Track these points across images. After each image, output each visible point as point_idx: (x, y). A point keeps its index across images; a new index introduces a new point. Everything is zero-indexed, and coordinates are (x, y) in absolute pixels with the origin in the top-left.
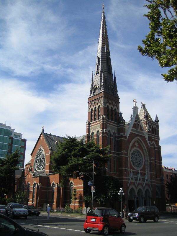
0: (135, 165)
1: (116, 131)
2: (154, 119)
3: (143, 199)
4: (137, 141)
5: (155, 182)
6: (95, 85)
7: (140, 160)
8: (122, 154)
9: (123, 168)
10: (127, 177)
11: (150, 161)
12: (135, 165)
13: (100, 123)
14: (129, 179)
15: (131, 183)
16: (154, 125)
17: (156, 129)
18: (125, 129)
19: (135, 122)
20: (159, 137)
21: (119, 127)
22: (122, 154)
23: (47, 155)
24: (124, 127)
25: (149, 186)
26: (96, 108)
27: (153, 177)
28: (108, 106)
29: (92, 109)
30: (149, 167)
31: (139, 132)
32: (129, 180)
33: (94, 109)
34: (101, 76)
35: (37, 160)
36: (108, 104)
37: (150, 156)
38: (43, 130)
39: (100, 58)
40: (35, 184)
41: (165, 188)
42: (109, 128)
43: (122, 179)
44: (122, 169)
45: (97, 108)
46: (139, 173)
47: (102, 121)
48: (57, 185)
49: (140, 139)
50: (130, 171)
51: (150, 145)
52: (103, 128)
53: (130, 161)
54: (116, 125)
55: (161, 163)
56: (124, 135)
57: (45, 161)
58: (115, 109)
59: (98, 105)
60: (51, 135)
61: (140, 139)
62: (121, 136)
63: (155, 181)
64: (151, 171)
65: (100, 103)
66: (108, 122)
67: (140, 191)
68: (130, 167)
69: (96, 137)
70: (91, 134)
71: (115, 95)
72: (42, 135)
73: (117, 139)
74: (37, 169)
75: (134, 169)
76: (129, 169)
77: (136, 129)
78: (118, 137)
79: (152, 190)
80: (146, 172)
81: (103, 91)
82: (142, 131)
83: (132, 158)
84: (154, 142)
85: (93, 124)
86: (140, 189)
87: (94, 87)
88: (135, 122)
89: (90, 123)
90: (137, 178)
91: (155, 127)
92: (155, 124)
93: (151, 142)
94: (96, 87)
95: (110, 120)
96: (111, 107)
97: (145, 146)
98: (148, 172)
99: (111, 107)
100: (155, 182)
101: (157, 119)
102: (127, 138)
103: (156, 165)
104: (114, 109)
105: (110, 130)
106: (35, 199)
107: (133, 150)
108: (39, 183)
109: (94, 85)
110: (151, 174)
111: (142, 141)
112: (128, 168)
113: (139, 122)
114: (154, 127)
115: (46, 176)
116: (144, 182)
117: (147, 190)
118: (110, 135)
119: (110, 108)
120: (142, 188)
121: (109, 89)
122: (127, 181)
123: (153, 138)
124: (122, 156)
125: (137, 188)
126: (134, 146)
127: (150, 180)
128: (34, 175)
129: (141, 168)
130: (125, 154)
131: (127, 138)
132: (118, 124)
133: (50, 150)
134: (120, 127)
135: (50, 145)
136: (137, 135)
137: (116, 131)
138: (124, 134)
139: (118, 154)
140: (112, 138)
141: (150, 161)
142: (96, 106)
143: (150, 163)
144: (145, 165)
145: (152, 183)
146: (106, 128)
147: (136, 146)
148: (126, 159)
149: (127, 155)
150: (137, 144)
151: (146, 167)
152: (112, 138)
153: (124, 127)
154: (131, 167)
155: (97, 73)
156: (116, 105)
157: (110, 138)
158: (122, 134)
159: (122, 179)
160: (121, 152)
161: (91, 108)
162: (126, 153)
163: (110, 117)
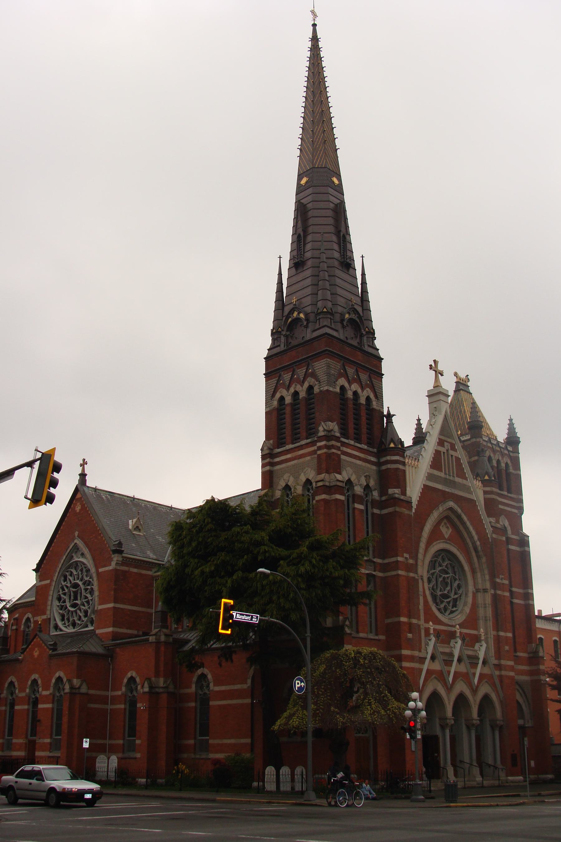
0: (442, 606)
1: (372, 483)
2: (501, 435)
3: (448, 732)
4: (447, 518)
5: (512, 669)
7: (459, 587)
8: (396, 566)
9: (403, 619)
10: (416, 653)
11: (492, 591)
12: (442, 606)
13: (315, 452)
14: (422, 660)
16: (503, 455)
17: (511, 470)
18: (404, 471)
19: (440, 449)
20: (521, 501)
21: (384, 467)
22: (396, 566)
23: (101, 570)
24: (401, 467)
25: (493, 685)
26: (296, 394)
27: (507, 648)
28: (342, 388)
29: (282, 399)
30: (490, 612)
31: (452, 484)
32: (423, 663)
33: (288, 400)
37: (493, 576)
38: (83, 476)
41: (548, 690)
43: (399, 658)
44: (399, 622)
48: (146, 685)
50: (427, 630)
51: (494, 532)
53: (424, 592)
54: (373, 459)
55: (529, 596)
56: (402, 497)
57: (96, 593)
58: (368, 399)
61: (459, 511)
62: (394, 501)
63: (511, 663)
64: (497, 627)
65: (314, 375)
66: (345, 449)
67: (461, 700)
71: (366, 348)
73: (376, 511)
74: (60, 624)
75: (437, 621)
76: (422, 622)
77: (442, 474)
78: (381, 505)
79: (501, 695)
80: (482, 630)
82: (464, 482)
83: (429, 581)
85: (289, 456)
87: (288, 317)
88: (440, 449)
90: (451, 655)
91: (507, 464)
92: (506, 452)
93: (497, 522)
94: (295, 314)
95: (352, 442)
96: (355, 393)
97: (474, 533)
98: (486, 634)
99: (355, 393)
100: (512, 669)
102: (414, 505)
103: (511, 603)
104: (363, 401)
105: (353, 478)
109: (287, 309)
110: (498, 639)
112: (419, 619)
114: (503, 465)
116: (451, 666)
117: (486, 698)
118: (354, 496)
120: (468, 693)
121: (345, 323)
122: (416, 665)
123: (501, 507)
124: (398, 575)
125: (449, 689)
126: (435, 535)
127: (496, 662)
129: (460, 618)
131: (414, 505)
132: (378, 455)
134: (389, 466)
136: (446, 496)
137: (372, 483)
138: (404, 493)
139: (384, 568)
140: (362, 507)
141: (492, 591)
142: (299, 388)
143: (495, 598)
145: (504, 673)
147: (444, 538)
148: (413, 583)
149: (413, 568)
150: (446, 531)
152: (362, 507)
153: (401, 467)
154: (430, 617)
156: (371, 382)
158: (394, 491)
159: (399, 658)
160: (393, 559)
161: (278, 395)
162: (411, 561)
163: (351, 431)
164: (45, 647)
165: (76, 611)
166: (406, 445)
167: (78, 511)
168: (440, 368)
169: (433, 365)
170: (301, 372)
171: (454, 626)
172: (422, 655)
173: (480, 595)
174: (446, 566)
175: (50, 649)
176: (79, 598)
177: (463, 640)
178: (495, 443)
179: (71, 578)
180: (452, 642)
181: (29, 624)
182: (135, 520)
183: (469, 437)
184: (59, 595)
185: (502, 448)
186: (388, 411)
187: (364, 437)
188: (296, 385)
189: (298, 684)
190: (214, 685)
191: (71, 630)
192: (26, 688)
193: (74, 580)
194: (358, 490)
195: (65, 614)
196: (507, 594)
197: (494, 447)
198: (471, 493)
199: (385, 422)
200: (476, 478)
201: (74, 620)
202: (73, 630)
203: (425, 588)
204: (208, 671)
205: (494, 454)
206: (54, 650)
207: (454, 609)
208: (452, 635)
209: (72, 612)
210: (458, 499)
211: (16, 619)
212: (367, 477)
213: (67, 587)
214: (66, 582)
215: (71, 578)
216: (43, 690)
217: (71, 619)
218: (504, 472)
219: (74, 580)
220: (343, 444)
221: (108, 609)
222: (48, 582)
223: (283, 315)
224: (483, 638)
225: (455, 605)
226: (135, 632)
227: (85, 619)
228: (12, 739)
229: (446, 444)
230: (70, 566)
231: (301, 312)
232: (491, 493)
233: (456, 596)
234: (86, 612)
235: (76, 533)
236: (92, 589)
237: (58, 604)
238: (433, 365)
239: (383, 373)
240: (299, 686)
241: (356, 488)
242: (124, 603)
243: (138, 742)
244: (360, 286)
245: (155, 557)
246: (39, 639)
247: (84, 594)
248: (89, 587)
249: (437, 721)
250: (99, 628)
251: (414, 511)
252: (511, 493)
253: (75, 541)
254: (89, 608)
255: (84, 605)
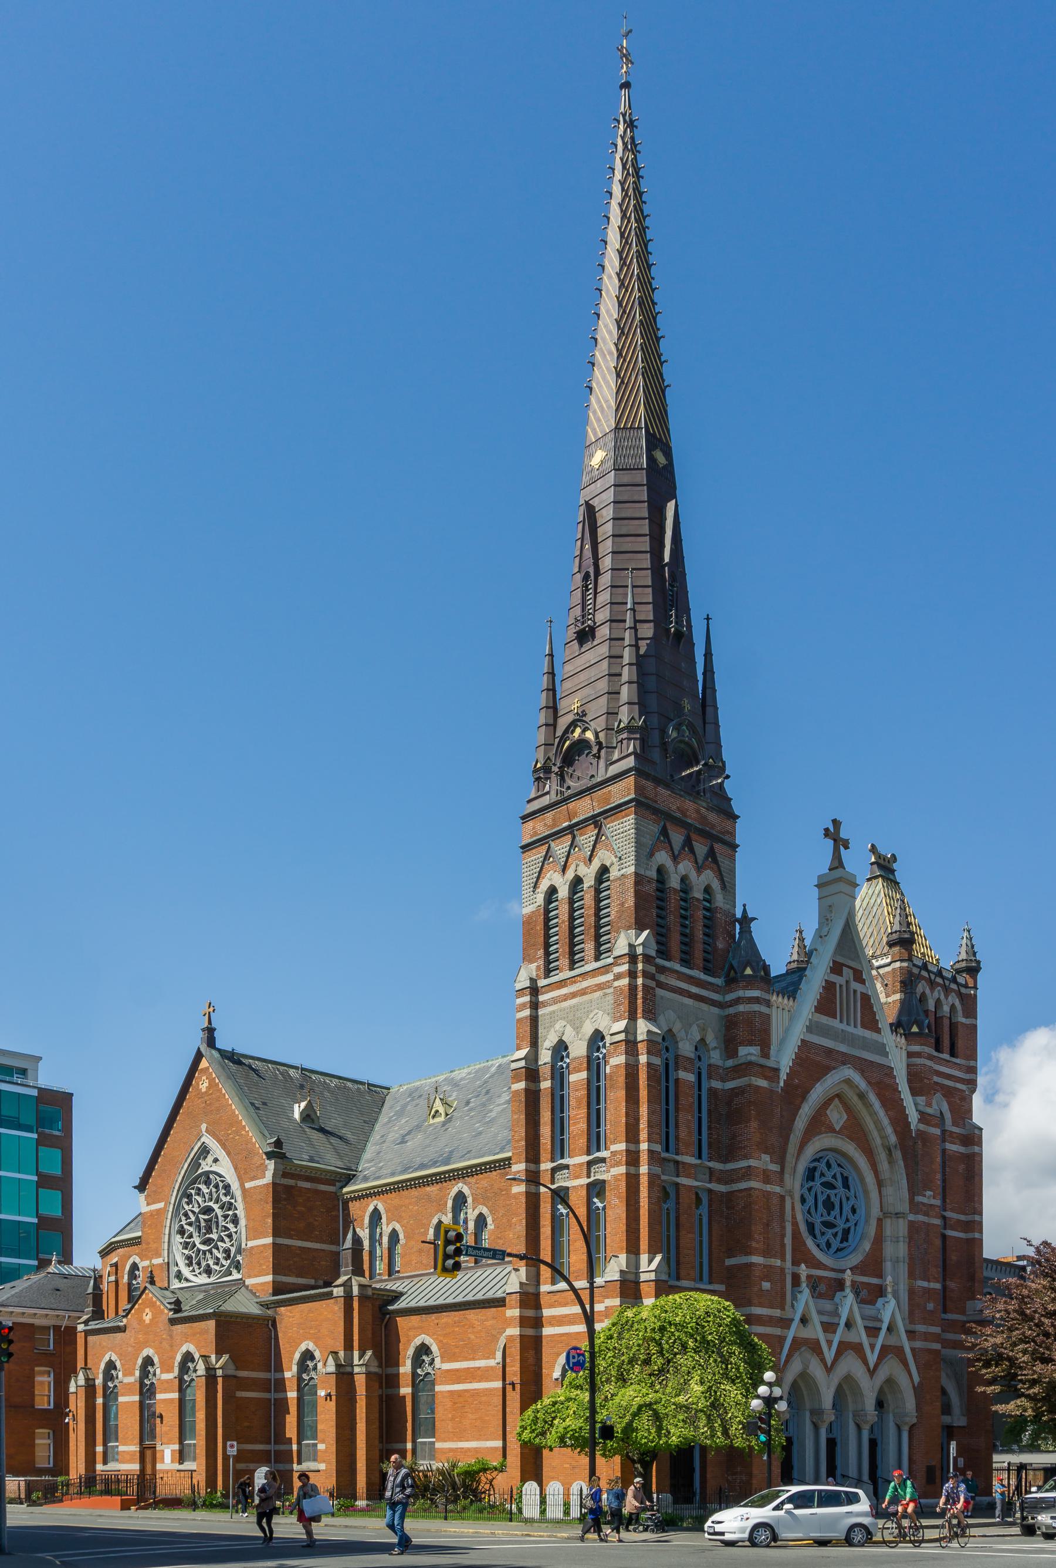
1: (711, 1039)
6: (573, 724)
8: (748, 1173)
9: (756, 1259)
14: (786, 1323)
15: (797, 1343)
16: (947, 990)
19: (834, 978)
22: (748, 1173)
23: (248, 1185)
24: (763, 1009)
26: (578, 881)
28: (660, 870)
29: (552, 890)
30: (902, 1250)
32: (788, 1327)
34: (615, 657)
35: (186, 1215)
36: (662, 857)
38: (210, 1031)
39: (606, 515)
40: (188, 1357)
42: (671, 1015)
45: (586, 885)
46: (848, 1283)
47: (625, 968)
48: (331, 1361)
49: (863, 1085)
50: (796, 1279)
51: (920, 1121)
52: (632, 1017)
57: (243, 1222)
58: (708, 890)
59: (596, 864)
60: (818, 1035)
63: (936, 1330)
64: (911, 1275)
67: (845, 1391)
68: (794, 1250)
69: (584, 1075)
70: (545, 1057)
72: (204, 1064)
74: (186, 1272)
79: (916, 1379)
80: (889, 1279)
81: (630, 762)
82: (874, 1036)
83: (803, 1200)
84: (940, 1105)
86: (848, 1379)
87: (563, 738)
88: (834, 978)
89: (542, 983)
90: (836, 1313)
91: (953, 1007)
96: (684, 879)
99: (684, 879)
101: (972, 951)
102: (783, 1076)
106: (198, 1442)
107: (810, 1151)
108: (219, 1353)
109: (563, 723)
110: (911, 1292)
111: (873, 1098)
113: (858, 976)
114: (946, 1008)
115: (255, 1310)
116: (834, 1332)
119: (674, 883)
126: (818, 1124)
128: (177, 1306)
129: (855, 1259)
130: (766, 1177)
131: (783, 1076)
133: (270, 1155)
134: (741, 1008)
135: (264, 1126)
136: (845, 1059)
138: (766, 1055)
144: (879, 1241)
146: (651, 1015)
151: (889, 1249)
153: (763, 1009)
154: (801, 1256)
155: (585, 636)
157: (672, 1076)
158: (748, 1052)
160: (743, 1164)
161: (544, 885)
164: (162, 1307)
165: (210, 1251)
166: (773, 973)
167: (204, 1090)
168: (843, 835)
169: (832, 829)
170: (586, 838)
171: (843, 1271)
172: (788, 1315)
173: (888, 1223)
174: (834, 1177)
175: (170, 1310)
176: (215, 1230)
177: (857, 1294)
178: (935, 970)
179: (200, 1199)
180: (880, 1301)
181: (137, 1273)
182: (303, 1105)
183: (889, 960)
184: (182, 1226)
185: (947, 979)
186: (745, 911)
187: (698, 955)
188: (577, 866)
189: (574, 1357)
190: (442, 1362)
191: (203, 1279)
192: (134, 1369)
193: (205, 1201)
194: (686, 1048)
195: (194, 1255)
196: (937, 1222)
197: (947, 983)
198: (886, 1055)
199: (738, 931)
200: (896, 1031)
201: (208, 1265)
202: (208, 1281)
203: (796, 1212)
204: (432, 1341)
205: (932, 989)
206: (178, 1310)
207: (845, 1244)
208: (840, 1285)
209: (204, 1252)
210: (863, 1066)
211: (116, 1265)
212: (703, 1029)
213: (193, 1212)
214: (191, 1206)
215: (200, 1199)
216: (162, 1372)
217: (204, 1264)
218: (946, 1022)
219: (205, 1201)
220: (662, 970)
221: (264, 1245)
222: (161, 1205)
223: (555, 735)
224: (889, 1289)
225: (845, 1238)
226: (312, 1282)
227: (226, 1263)
228: (117, 1447)
229: (845, 969)
230: (194, 1182)
231: (589, 729)
232: (918, 1055)
233: (847, 1226)
234: (227, 1252)
235: (204, 1127)
236: (235, 1215)
237: (182, 1240)
238: (832, 829)
239: (737, 842)
240: (575, 1360)
241: (680, 1045)
242: (291, 1237)
243: (321, 1447)
244: (700, 678)
245: (340, 1164)
246: (151, 1295)
247: (223, 1224)
248: (231, 1213)
249: (808, 1414)
250: (250, 1277)
251: (782, 1084)
252: (957, 1057)
253: (202, 1140)
254: (232, 1245)
255: (223, 1241)
